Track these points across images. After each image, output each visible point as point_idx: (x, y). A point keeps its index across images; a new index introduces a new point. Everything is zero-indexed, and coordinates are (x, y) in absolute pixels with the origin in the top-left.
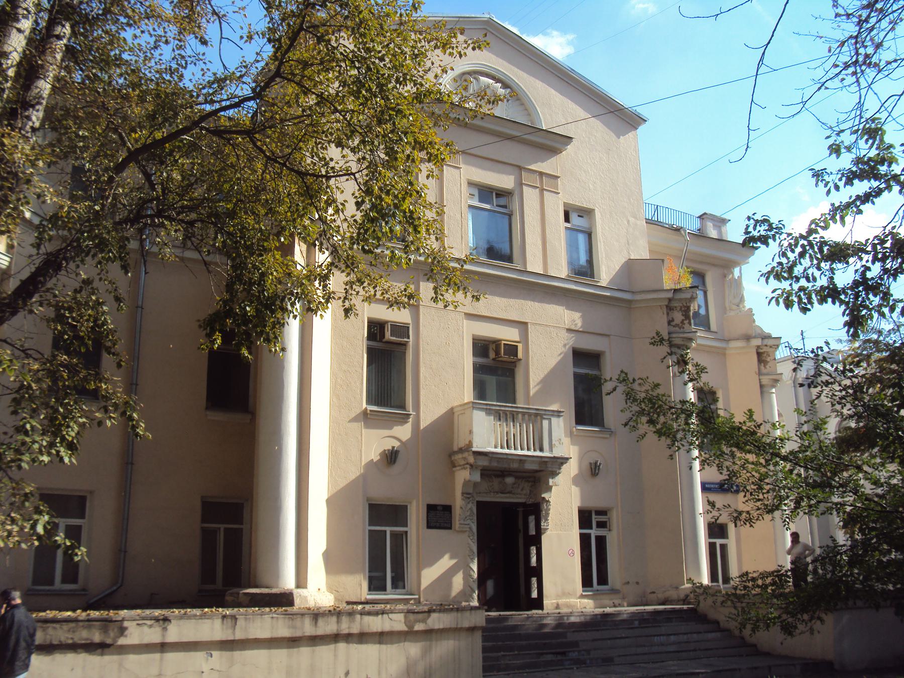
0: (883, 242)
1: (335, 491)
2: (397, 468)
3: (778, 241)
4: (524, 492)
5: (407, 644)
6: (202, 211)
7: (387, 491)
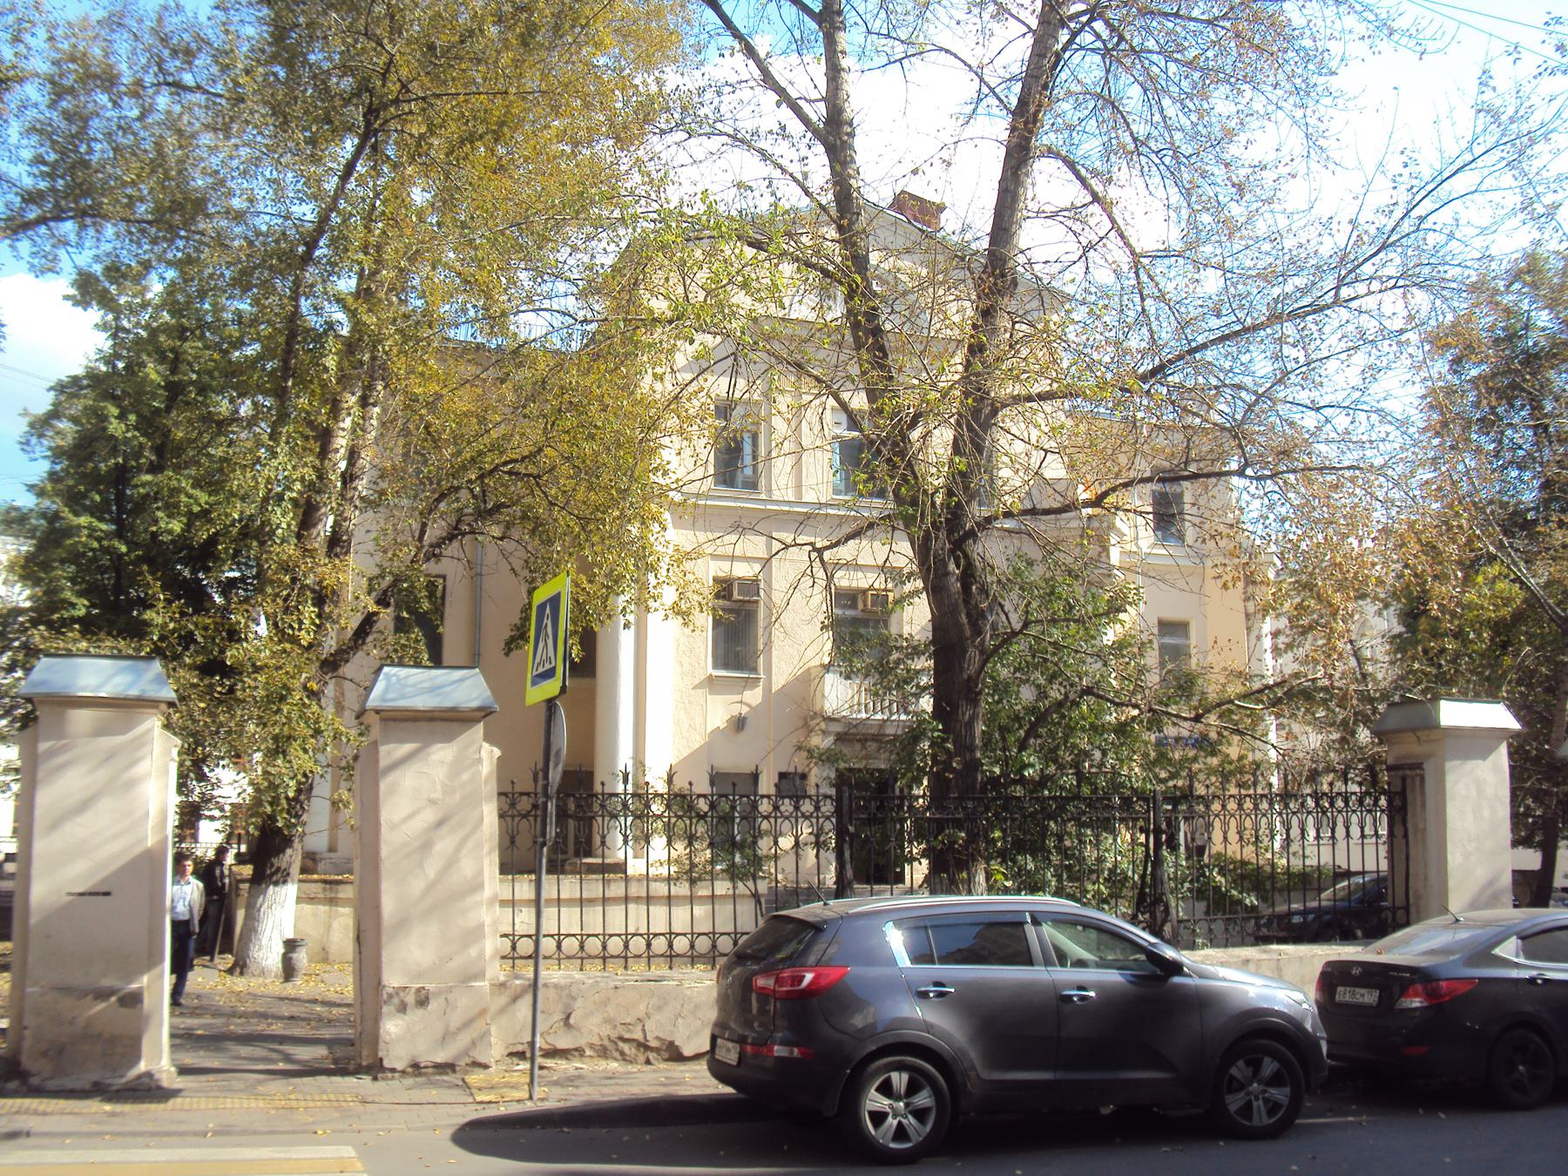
2: (743, 736)
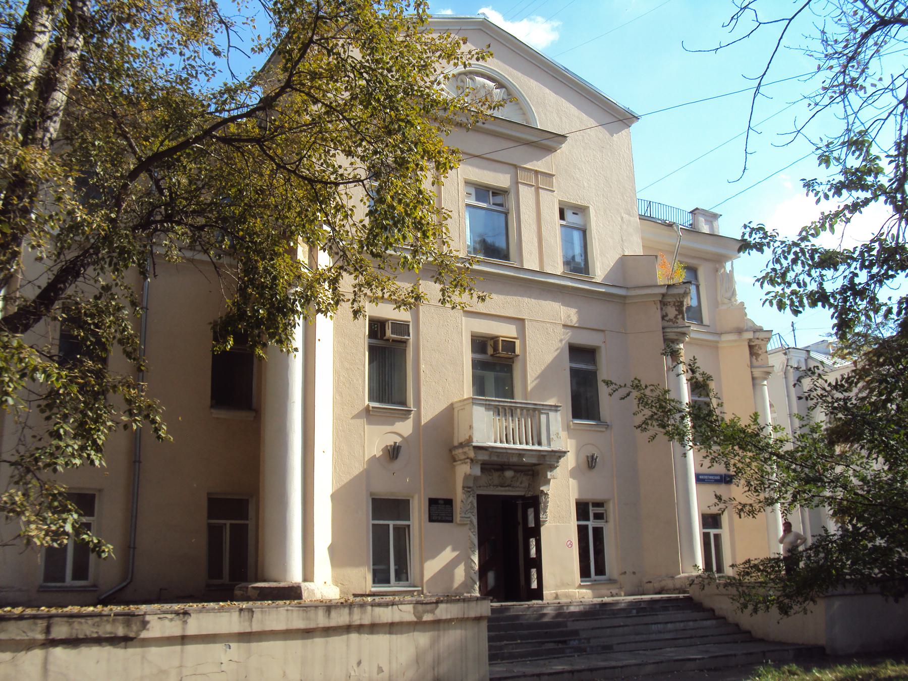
0: (870, 249)
1: (339, 486)
3: (772, 248)
4: (523, 485)
5: (416, 634)
6: (210, 215)
7: (387, 488)
